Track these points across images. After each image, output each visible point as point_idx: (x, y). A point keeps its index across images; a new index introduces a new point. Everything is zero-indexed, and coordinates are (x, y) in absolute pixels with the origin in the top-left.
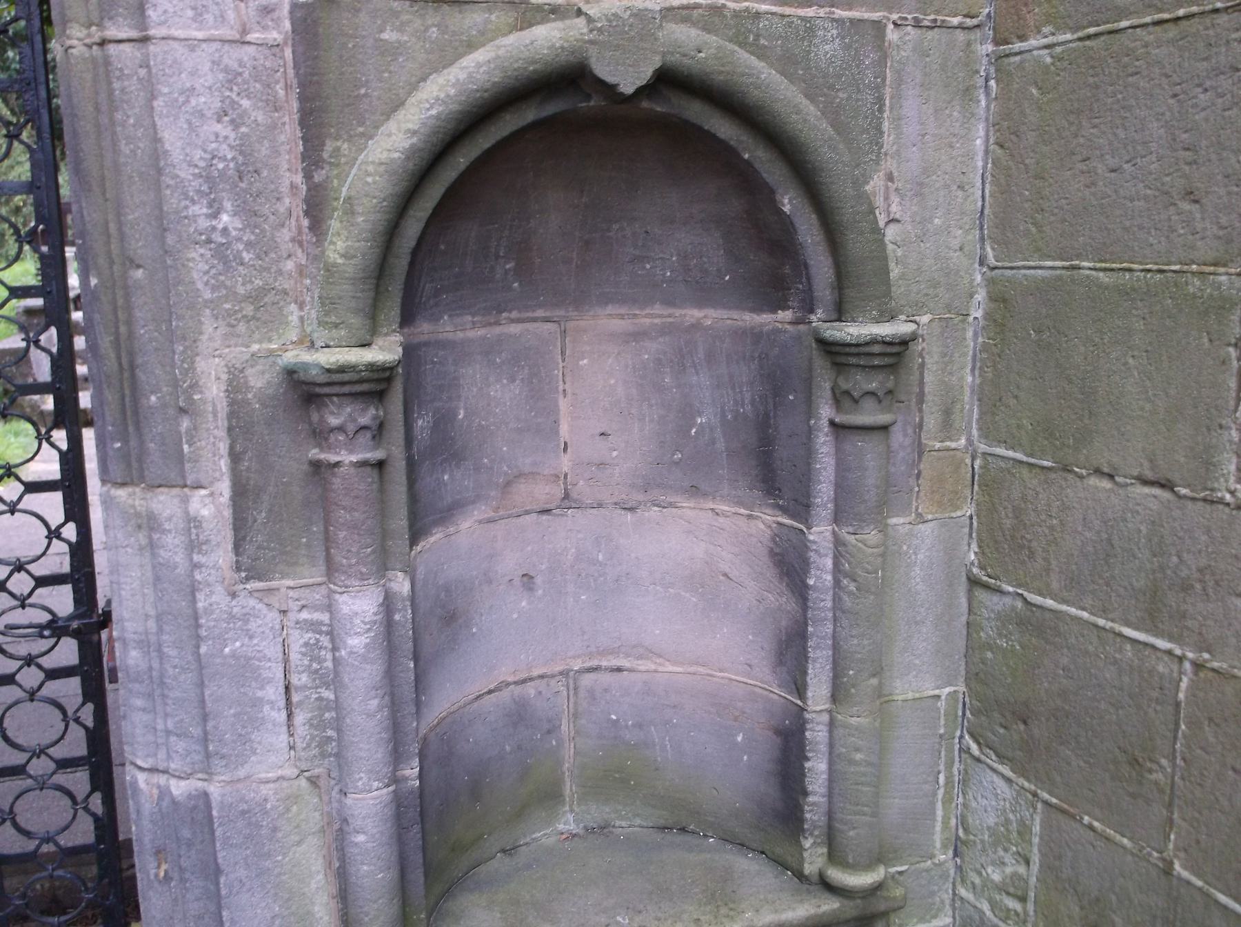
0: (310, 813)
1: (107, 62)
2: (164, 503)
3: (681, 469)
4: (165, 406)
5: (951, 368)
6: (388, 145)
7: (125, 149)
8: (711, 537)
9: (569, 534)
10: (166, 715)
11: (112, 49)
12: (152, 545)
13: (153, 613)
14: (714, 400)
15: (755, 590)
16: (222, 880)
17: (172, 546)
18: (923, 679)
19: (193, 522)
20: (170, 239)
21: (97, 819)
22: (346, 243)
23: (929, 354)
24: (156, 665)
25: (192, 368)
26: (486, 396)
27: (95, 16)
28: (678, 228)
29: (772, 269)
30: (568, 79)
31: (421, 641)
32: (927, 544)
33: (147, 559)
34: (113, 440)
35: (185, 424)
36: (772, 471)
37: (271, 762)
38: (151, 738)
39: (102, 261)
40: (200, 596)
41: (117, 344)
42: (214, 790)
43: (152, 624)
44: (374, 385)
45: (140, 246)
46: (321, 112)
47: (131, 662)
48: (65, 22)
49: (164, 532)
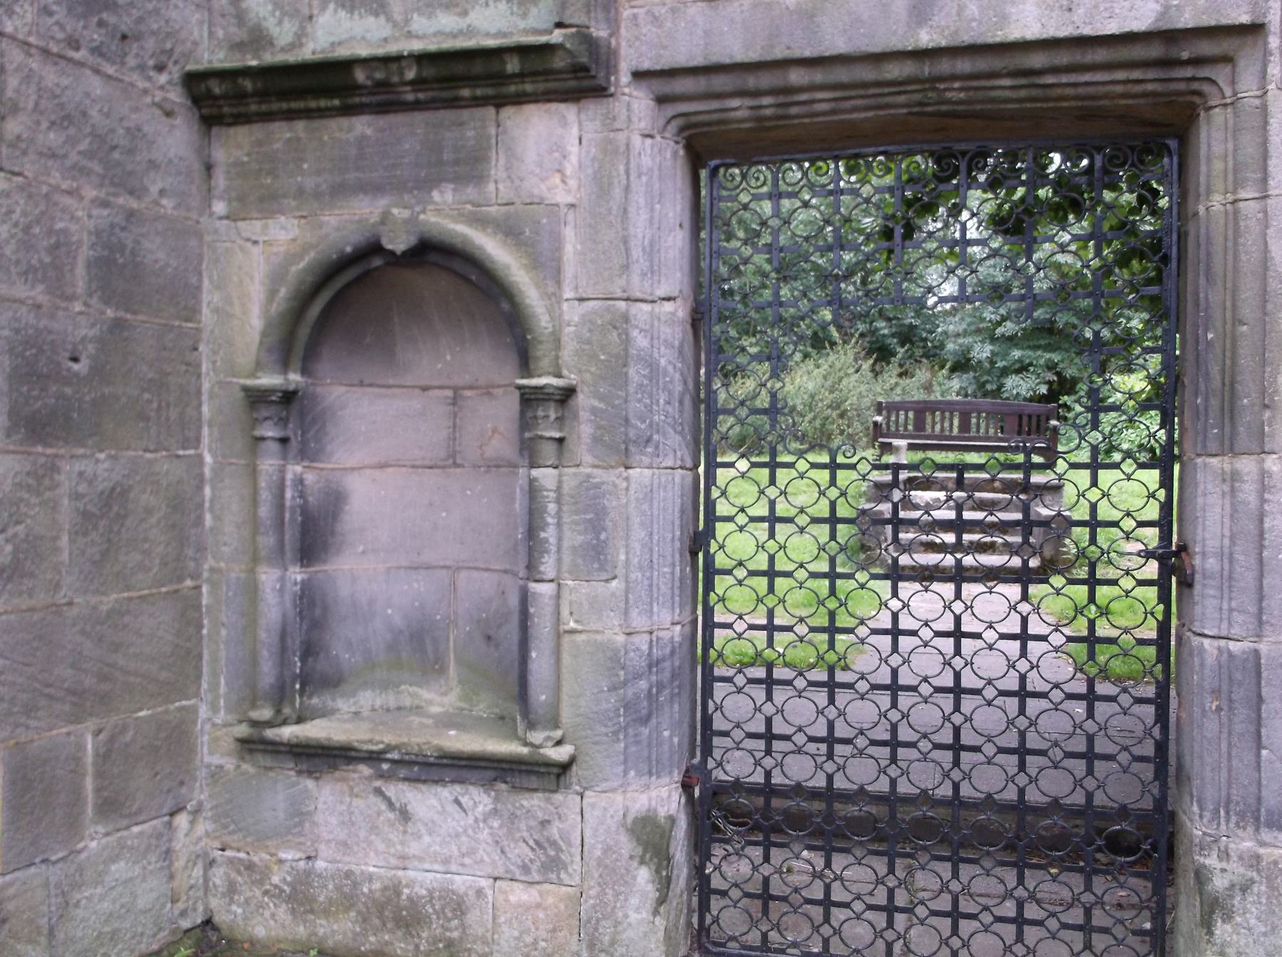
1: (1236, 212)
2: (1247, 465)
4: (1253, 405)
7: (1243, 257)
10: (1231, 599)
11: (1241, 204)
12: (1233, 490)
13: (1227, 533)
16: (1264, 707)
17: (1248, 492)
19: (1263, 474)
20: (1270, 307)
21: (1157, 682)
24: (1226, 566)
25: (1275, 381)
27: (1231, 188)
33: (1227, 502)
34: (1213, 428)
35: (1267, 414)
38: (1217, 615)
39: (1218, 324)
40: (1267, 520)
41: (1223, 371)
42: (1263, 647)
43: (1227, 542)
45: (1248, 311)
47: (1208, 566)
48: (1209, 192)
49: (1243, 481)
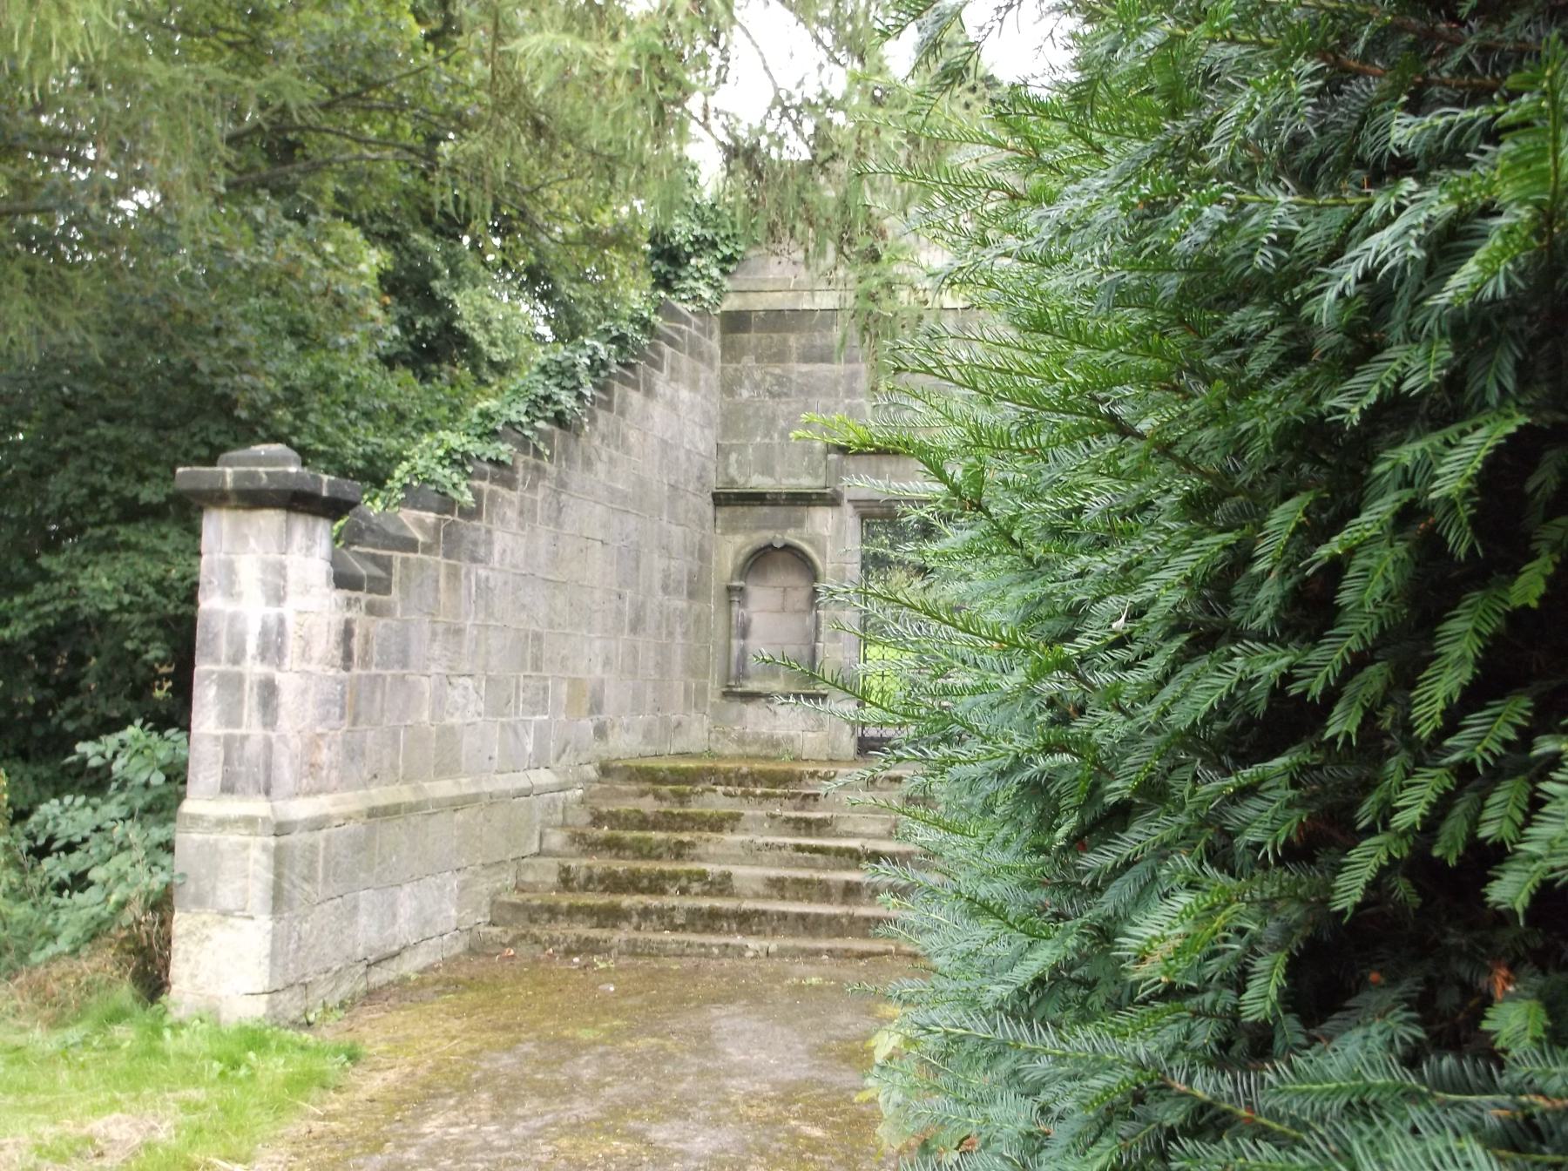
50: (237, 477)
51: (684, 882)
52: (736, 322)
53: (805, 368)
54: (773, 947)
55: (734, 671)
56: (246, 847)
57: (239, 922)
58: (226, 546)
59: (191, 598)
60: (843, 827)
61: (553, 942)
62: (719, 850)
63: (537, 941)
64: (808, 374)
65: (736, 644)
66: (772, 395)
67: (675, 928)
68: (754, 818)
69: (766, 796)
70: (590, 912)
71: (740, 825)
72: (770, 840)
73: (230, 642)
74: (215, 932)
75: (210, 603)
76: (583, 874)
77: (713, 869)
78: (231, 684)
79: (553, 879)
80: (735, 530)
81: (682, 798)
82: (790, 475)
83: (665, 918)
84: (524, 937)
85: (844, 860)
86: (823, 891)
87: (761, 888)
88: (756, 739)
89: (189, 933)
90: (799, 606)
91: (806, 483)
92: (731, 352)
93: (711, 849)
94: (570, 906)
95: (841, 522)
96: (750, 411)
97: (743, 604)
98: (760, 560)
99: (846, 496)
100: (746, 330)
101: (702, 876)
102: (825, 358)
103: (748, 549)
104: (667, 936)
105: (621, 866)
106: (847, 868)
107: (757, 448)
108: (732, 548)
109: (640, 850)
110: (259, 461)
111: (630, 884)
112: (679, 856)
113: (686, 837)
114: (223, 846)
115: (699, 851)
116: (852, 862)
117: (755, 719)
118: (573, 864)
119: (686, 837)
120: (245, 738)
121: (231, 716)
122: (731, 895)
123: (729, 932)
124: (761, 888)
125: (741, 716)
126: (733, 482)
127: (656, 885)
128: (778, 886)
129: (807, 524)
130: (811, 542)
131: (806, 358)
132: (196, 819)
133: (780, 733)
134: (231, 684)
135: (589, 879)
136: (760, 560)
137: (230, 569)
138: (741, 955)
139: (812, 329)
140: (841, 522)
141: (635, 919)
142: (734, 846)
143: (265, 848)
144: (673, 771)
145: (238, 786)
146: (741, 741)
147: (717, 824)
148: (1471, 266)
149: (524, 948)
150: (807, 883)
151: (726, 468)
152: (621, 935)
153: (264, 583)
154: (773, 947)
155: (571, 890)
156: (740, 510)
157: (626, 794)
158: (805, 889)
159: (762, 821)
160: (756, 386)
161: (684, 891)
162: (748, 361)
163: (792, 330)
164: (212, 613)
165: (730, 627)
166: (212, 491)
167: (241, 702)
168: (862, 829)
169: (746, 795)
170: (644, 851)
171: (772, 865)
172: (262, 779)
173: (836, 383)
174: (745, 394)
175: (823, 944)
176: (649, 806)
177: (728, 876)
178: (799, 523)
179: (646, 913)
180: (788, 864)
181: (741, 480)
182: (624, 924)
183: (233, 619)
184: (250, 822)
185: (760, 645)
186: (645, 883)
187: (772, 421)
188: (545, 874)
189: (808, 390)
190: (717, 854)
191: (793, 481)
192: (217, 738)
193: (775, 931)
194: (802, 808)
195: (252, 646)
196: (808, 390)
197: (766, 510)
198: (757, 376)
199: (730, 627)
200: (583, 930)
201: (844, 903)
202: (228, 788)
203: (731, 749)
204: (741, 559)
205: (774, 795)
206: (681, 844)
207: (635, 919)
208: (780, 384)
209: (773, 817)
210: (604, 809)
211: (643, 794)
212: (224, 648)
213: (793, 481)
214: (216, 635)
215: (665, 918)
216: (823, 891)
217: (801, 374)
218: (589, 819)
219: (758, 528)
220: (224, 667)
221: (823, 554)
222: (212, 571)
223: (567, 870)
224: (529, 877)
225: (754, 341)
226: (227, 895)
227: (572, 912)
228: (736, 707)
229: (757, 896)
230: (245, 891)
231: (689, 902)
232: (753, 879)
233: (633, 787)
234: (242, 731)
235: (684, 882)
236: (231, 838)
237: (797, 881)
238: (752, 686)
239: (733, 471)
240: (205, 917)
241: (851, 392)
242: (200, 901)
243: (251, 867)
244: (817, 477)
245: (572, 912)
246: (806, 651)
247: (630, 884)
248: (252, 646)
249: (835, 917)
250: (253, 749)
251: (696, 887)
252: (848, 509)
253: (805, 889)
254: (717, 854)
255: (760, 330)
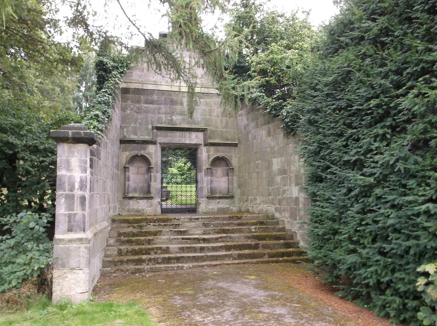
0: (206, 187)
3: (224, 176)
5: (236, 170)
6: (211, 159)
8: (225, 179)
9: (218, 179)
14: (225, 172)
15: (227, 181)
18: (235, 185)
22: (209, 163)
23: (235, 169)
26: (214, 171)
28: (223, 164)
29: (227, 165)
30: (218, 157)
31: (212, 182)
32: (235, 178)
36: (228, 175)
37: (205, 185)
44: (210, 168)
46: (209, 158)
50: (73, 133)
51: (155, 250)
52: (126, 91)
53: (146, 105)
54: (191, 266)
55: (126, 191)
56: (79, 248)
57: (77, 271)
58: (66, 154)
59: (54, 171)
60: (190, 232)
61: (127, 270)
62: (161, 241)
63: (122, 271)
64: (147, 107)
65: (127, 183)
66: (136, 112)
67: (159, 263)
68: (166, 232)
69: (165, 225)
70: (133, 261)
71: (162, 234)
72: (175, 237)
73: (69, 185)
74: (69, 276)
75: (61, 172)
76: (125, 250)
77: (164, 246)
78: (70, 198)
79: (116, 253)
80: (126, 151)
81: (141, 227)
82: (142, 135)
83: (155, 261)
84: (118, 270)
85: (195, 241)
86: (194, 250)
87: (177, 250)
88: (133, 210)
89: (59, 276)
90: (143, 172)
91: (147, 138)
92: (124, 100)
93: (158, 241)
94: (127, 260)
95: (157, 149)
96: (130, 117)
97: (128, 172)
98: (133, 159)
99: (158, 141)
100: (129, 94)
101: (160, 248)
102: (152, 103)
103: (130, 156)
104: (157, 266)
105: (137, 248)
106: (196, 243)
107: (132, 127)
108: (126, 155)
109: (137, 243)
110: (70, 128)
111: (140, 252)
112: (149, 244)
113: (151, 238)
114: (71, 248)
115: (155, 242)
116: (198, 242)
117: (134, 205)
118: (122, 248)
119: (151, 238)
120: (75, 214)
121: (70, 207)
122: (169, 253)
123: (174, 263)
124: (177, 250)
125: (128, 203)
126: (125, 137)
127: (147, 252)
128: (182, 250)
129: (147, 149)
130: (148, 154)
131: (146, 103)
132: (61, 240)
133: (140, 208)
134: (70, 198)
135: (127, 252)
136: (133, 159)
137: (68, 163)
138: (182, 269)
139: (147, 95)
140: (157, 149)
141: (147, 262)
142: (164, 239)
143: (86, 248)
144: (134, 220)
145: (74, 229)
146: (128, 211)
147: (155, 234)
148: (401, 90)
149: (118, 274)
150: (190, 248)
151: (123, 133)
152: (145, 266)
153: (80, 166)
154: (191, 266)
155: (122, 256)
156: (127, 145)
157: (124, 227)
158: (190, 250)
159: (168, 232)
160: (132, 110)
161: (156, 253)
162: (129, 102)
163: (142, 94)
164: (62, 175)
165: (125, 178)
166: (64, 137)
167: (74, 203)
168: (196, 232)
169: (159, 225)
170: (138, 243)
171: (176, 244)
172: (82, 226)
173: (155, 110)
174: (128, 112)
175: (204, 263)
176: (131, 229)
177: (168, 248)
178: (145, 149)
179: (150, 260)
180: (180, 243)
181: (128, 136)
182: (144, 264)
183: (70, 177)
184: (81, 240)
185: (132, 184)
186: (144, 251)
187: (136, 120)
188: (114, 251)
189: (147, 112)
190: (162, 241)
191: (143, 137)
192: (65, 215)
193: (187, 262)
194: (175, 228)
195: (77, 186)
196: (147, 112)
197: (135, 145)
198: (132, 107)
199: (125, 178)
200: (132, 267)
201: (200, 252)
202: (70, 230)
203: (126, 213)
204: (128, 159)
205: (167, 225)
206: (150, 240)
207: (147, 262)
208: (139, 110)
209: (171, 231)
210: (121, 232)
211: (129, 227)
212: (67, 186)
213: (143, 137)
214: (64, 183)
215: (155, 261)
216: (194, 250)
217: (145, 107)
218: (117, 235)
219: (133, 150)
220: (67, 192)
221: (152, 158)
222: (61, 163)
223: (120, 250)
224: (109, 253)
225: (131, 97)
226: (73, 263)
227: (128, 262)
228: (127, 201)
229: (177, 253)
230: (79, 261)
231: (162, 256)
232: (175, 248)
233: (126, 225)
234: (75, 212)
235: (155, 250)
236: (75, 245)
237: (187, 248)
238: (130, 195)
239: (125, 134)
240: (65, 271)
241: (159, 113)
242: (63, 266)
243: (81, 253)
244: (150, 136)
245: (128, 262)
246: (145, 185)
247: (140, 252)
248: (77, 186)
249: (203, 256)
250: (78, 218)
251: (159, 252)
252: (158, 145)
253: (190, 250)
254: (162, 241)
255: (132, 94)
